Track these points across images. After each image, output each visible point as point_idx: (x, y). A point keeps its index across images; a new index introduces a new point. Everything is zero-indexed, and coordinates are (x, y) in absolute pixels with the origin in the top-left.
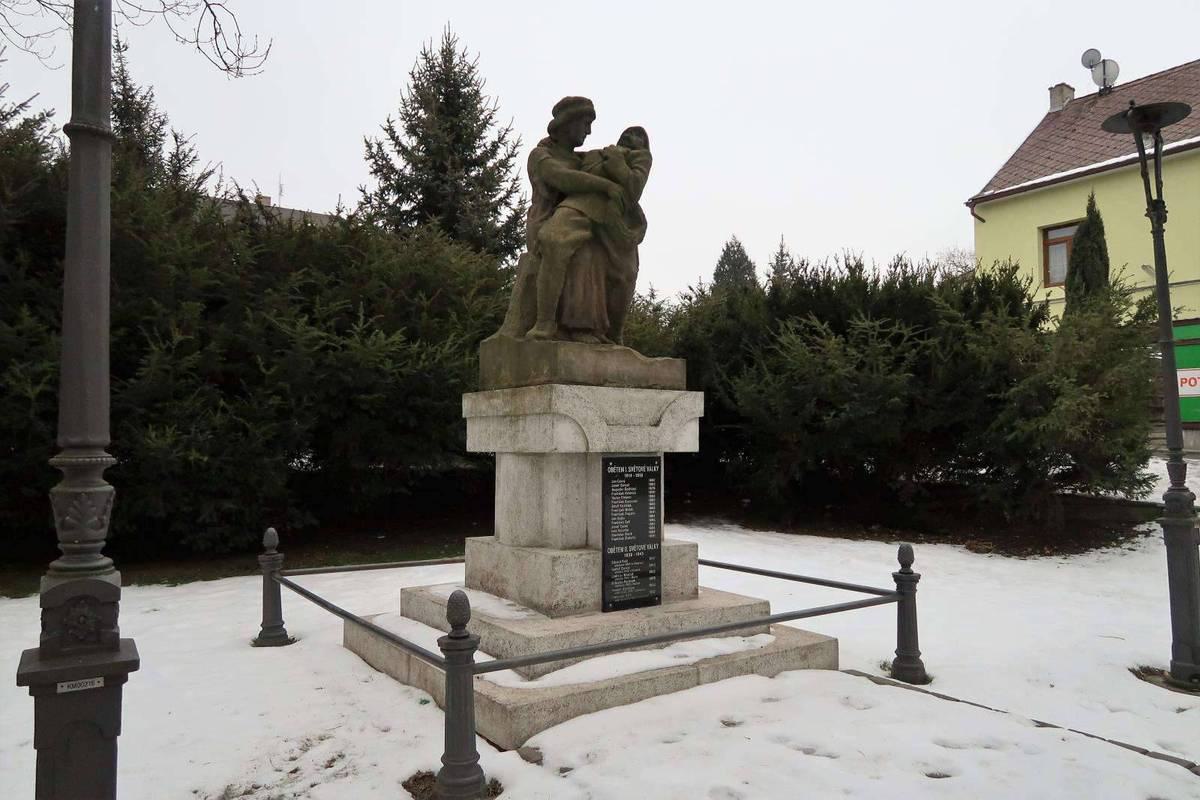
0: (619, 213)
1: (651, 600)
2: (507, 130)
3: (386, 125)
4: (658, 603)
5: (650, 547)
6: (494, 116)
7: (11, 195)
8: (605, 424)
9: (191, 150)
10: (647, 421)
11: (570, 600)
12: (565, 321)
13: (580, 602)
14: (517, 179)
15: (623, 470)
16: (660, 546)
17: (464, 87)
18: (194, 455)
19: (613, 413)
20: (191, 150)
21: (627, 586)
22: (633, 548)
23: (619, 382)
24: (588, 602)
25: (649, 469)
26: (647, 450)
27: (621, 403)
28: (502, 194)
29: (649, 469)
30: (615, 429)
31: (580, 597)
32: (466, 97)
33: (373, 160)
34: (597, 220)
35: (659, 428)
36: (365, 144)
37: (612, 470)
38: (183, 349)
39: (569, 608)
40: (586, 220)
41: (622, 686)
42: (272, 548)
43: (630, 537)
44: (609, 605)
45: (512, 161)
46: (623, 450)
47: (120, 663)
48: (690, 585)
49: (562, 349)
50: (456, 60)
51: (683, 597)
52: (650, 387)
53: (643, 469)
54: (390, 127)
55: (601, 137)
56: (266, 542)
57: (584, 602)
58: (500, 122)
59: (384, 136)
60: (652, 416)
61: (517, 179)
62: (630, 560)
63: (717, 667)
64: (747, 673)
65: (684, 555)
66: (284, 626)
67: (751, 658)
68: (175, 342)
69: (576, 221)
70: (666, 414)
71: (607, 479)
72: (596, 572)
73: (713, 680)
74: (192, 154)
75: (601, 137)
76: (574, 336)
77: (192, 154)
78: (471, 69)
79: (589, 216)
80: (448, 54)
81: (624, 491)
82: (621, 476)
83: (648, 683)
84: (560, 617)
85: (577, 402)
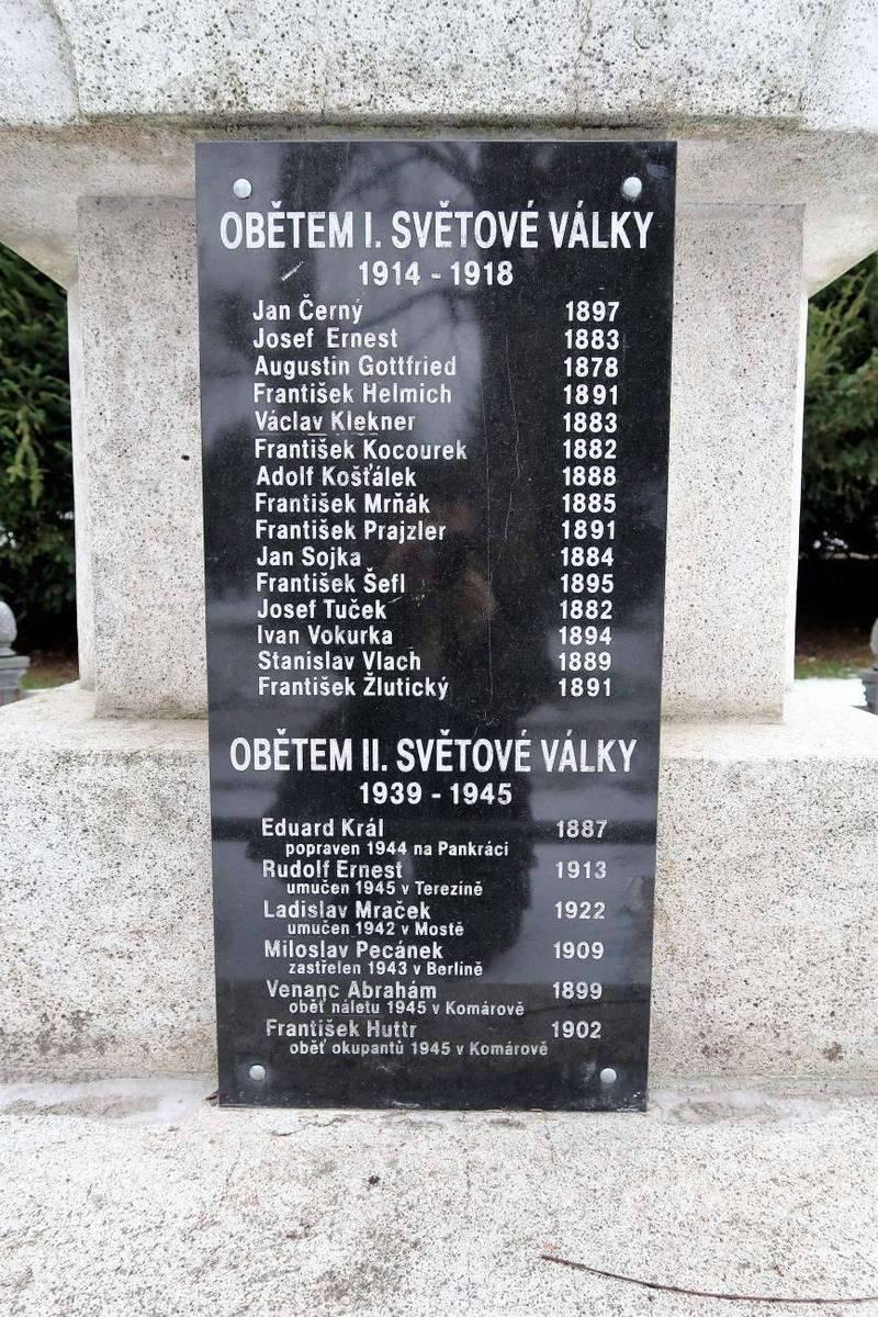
4: (632, 1093)
22: (432, 753)
24: (133, 1025)
25: (573, 230)
29: (573, 230)
57: (100, 1025)
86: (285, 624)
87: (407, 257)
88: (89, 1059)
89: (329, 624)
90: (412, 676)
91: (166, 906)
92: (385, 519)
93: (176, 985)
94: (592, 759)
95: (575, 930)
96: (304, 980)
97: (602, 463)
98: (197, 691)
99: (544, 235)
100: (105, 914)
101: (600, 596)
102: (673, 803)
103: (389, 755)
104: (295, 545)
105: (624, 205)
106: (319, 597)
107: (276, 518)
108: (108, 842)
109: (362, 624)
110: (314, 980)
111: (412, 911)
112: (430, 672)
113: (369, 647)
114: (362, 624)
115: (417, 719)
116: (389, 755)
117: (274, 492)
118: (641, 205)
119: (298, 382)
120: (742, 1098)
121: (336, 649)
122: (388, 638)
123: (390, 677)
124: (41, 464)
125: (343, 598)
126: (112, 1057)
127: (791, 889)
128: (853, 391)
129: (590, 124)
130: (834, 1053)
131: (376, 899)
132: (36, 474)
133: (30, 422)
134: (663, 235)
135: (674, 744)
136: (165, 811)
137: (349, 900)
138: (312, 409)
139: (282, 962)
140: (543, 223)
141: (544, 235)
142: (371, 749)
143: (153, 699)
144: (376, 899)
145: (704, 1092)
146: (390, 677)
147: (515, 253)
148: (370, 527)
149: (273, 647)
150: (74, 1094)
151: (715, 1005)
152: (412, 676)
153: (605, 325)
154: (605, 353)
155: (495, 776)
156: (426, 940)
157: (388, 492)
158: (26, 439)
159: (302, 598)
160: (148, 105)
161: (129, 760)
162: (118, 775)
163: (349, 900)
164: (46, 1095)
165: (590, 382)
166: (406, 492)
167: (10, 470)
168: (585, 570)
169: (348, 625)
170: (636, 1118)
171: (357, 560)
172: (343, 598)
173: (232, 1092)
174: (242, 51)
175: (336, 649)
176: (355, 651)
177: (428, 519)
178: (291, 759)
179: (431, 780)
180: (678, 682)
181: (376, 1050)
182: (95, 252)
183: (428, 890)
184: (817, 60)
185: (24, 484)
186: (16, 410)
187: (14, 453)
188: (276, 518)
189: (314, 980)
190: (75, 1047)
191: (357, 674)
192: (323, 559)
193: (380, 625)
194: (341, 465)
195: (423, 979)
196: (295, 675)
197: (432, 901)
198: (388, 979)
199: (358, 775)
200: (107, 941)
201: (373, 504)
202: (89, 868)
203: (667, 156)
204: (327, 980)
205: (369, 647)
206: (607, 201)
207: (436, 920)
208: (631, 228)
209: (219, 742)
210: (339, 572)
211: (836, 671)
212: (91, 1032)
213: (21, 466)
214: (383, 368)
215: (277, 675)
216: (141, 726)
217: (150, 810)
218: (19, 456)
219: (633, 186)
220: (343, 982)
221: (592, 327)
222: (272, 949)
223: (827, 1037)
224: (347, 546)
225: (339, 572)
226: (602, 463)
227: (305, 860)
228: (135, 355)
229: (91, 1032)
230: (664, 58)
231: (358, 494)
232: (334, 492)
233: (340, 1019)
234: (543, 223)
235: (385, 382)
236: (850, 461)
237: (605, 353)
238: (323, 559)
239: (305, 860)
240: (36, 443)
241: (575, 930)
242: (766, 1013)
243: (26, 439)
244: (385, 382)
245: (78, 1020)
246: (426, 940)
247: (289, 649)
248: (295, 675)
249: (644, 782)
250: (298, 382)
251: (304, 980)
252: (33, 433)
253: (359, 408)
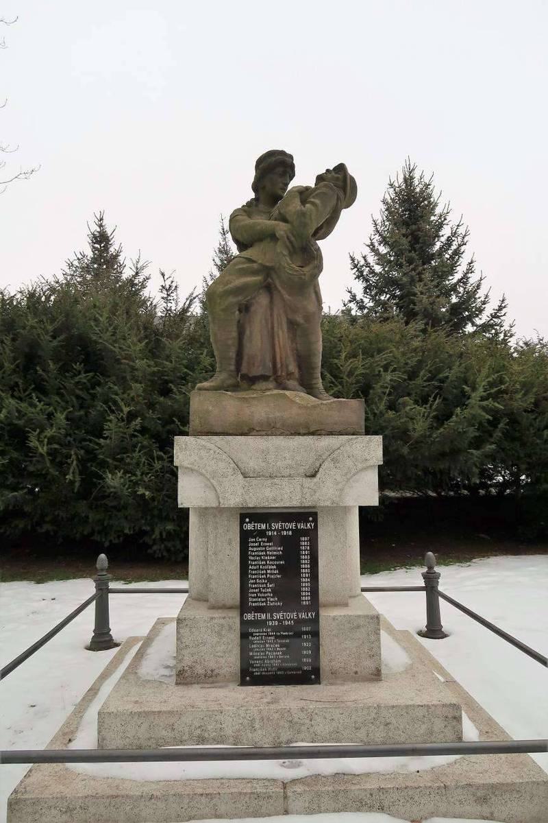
0: (285, 253)
1: (309, 676)
2: (458, 226)
3: (368, 242)
4: (317, 681)
5: (303, 616)
6: (447, 217)
7: (50, 327)
8: (241, 477)
9: (172, 282)
10: (301, 470)
11: (198, 666)
12: (244, 370)
13: (212, 671)
14: (472, 263)
15: (263, 527)
16: (317, 615)
17: (423, 201)
18: (141, 491)
19: (252, 464)
20: (172, 282)
21: (272, 654)
22: (279, 616)
23: (269, 429)
24: (222, 672)
25: (301, 526)
26: (298, 505)
27: (265, 452)
28: (457, 276)
29: (301, 526)
30: (254, 482)
31: (212, 665)
32: (424, 207)
33: (356, 269)
34: (267, 264)
35: (315, 480)
36: (350, 259)
37: (249, 527)
38: (132, 416)
39: (198, 676)
40: (255, 266)
41: (165, 798)
42: (102, 570)
43: (273, 601)
44: (250, 676)
45: (463, 248)
46: (266, 504)
47: (438, 576)
48: (369, 664)
49: (197, 399)
50: (416, 182)
51: (357, 677)
52: (313, 434)
53: (292, 525)
54: (371, 243)
55: (304, 177)
56: (98, 566)
57: (217, 671)
58: (452, 220)
59: (367, 251)
60: (306, 468)
61: (472, 263)
62: (274, 629)
63: (319, 795)
64: (371, 808)
65: (358, 627)
66: (111, 633)
67: (380, 789)
68: (125, 413)
69: (243, 269)
70: (326, 463)
71: (245, 536)
72: (234, 637)
73: (310, 811)
74: (174, 284)
75: (304, 177)
76: (254, 383)
77: (174, 284)
78: (427, 186)
79: (260, 262)
80: (409, 180)
81: (266, 551)
82: (262, 533)
83: (203, 799)
84: (186, 684)
85: (203, 453)
86: (254, 593)
87: (274, 530)
88: (214, 679)
89: (262, 593)
90: (275, 601)
91: (230, 647)
92: (271, 574)
93: (230, 661)
94: (308, 616)
95: (307, 648)
96: (256, 660)
97: (307, 564)
98: (238, 603)
99: (296, 526)
100: (218, 648)
101: (308, 587)
102: (322, 622)
103: (272, 616)
104: (256, 579)
105: (310, 522)
106: (260, 588)
107: (252, 574)
108: (219, 634)
109: (267, 593)
110: (259, 660)
111: (276, 646)
112: (279, 600)
113: (268, 597)
114: (267, 593)
115: (277, 609)
116: (272, 616)
117: (252, 570)
118: (312, 522)
119: (256, 551)
120: (338, 682)
121: (263, 597)
122: (272, 595)
123: (272, 602)
124: (81, 474)
125: (264, 588)
126: (219, 678)
127: (345, 639)
128: (437, 440)
129: (305, 507)
130: (356, 673)
131: (270, 643)
132: (78, 478)
133: (76, 454)
134: (316, 526)
135: (324, 614)
136: (230, 628)
137: (264, 644)
138: (258, 556)
139: (253, 656)
140: (296, 525)
141: (296, 526)
142: (269, 615)
143: (220, 605)
144: (270, 643)
145: (331, 681)
146: (272, 602)
147: (292, 530)
148: (268, 576)
149: (252, 597)
150: (212, 685)
151: (333, 663)
152: (275, 601)
153: (307, 541)
154: (307, 546)
155: (289, 530)
156: (279, 651)
157: (271, 569)
158: (75, 463)
159: (255, 588)
160: (232, 506)
161: (224, 618)
162: (222, 621)
163: (264, 644)
164: (206, 685)
165: (305, 550)
166: (274, 569)
167: (67, 477)
168: (305, 582)
169: (265, 593)
170: (318, 685)
171: (266, 581)
172: (264, 588)
173: (243, 683)
174: (247, 497)
175: (263, 597)
176: (266, 597)
177: (278, 574)
178: (254, 618)
179: (279, 621)
180: (322, 598)
181: (270, 673)
182: (212, 517)
183: (279, 641)
184: (340, 496)
185: (72, 482)
186: (71, 450)
187: (69, 469)
188: (252, 574)
189: (259, 660)
190: (211, 676)
191: (267, 601)
192: (260, 581)
193: (270, 593)
194: (264, 565)
195: (278, 659)
196: (255, 602)
197: (280, 643)
198: (272, 659)
199: (266, 620)
200: (219, 654)
201: (268, 572)
202: (216, 639)
203: (315, 515)
204: (261, 659)
205: (268, 597)
206: (307, 521)
207: (281, 647)
208: (311, 525)
209: (242, 615)
210: (263, 583)
211: (444, 561)
212: (215, 673)
213: (71, 475)
214: (270, 549)
215: (253, 602)
216: (220, 611)
217: (227, 628)
218: (71, 471)
219: (311, 519)
220: (264, 660)
221: (304, 542)
222: (251, 654)
223: (355, 669)
224: (264, 579)
225: (263, 583)
226: (307, 564)
227: (257, 636)
228: (219, 535)
229: (215, 673)
230: (315, 497)
231: (266, 570)
232: (262, 570)
233: (263, 667)
234: (296, 525)
235: (270, 551)
236: (442, 467)
237: (307, 546)
238: (260, 581)
239: (257, 636)
240: (79, 464)
241: (307, 648)
242: (342, 665)
243: (75, 463)
244: (270, 551)
245: (212, 671)
246: (279, 651)
247: (254, 597)
248: (255, 602)
249: (316, 621)
250: (256, 551)
251: (256, 660)
252: (78, 459)
253: (267, 555)
